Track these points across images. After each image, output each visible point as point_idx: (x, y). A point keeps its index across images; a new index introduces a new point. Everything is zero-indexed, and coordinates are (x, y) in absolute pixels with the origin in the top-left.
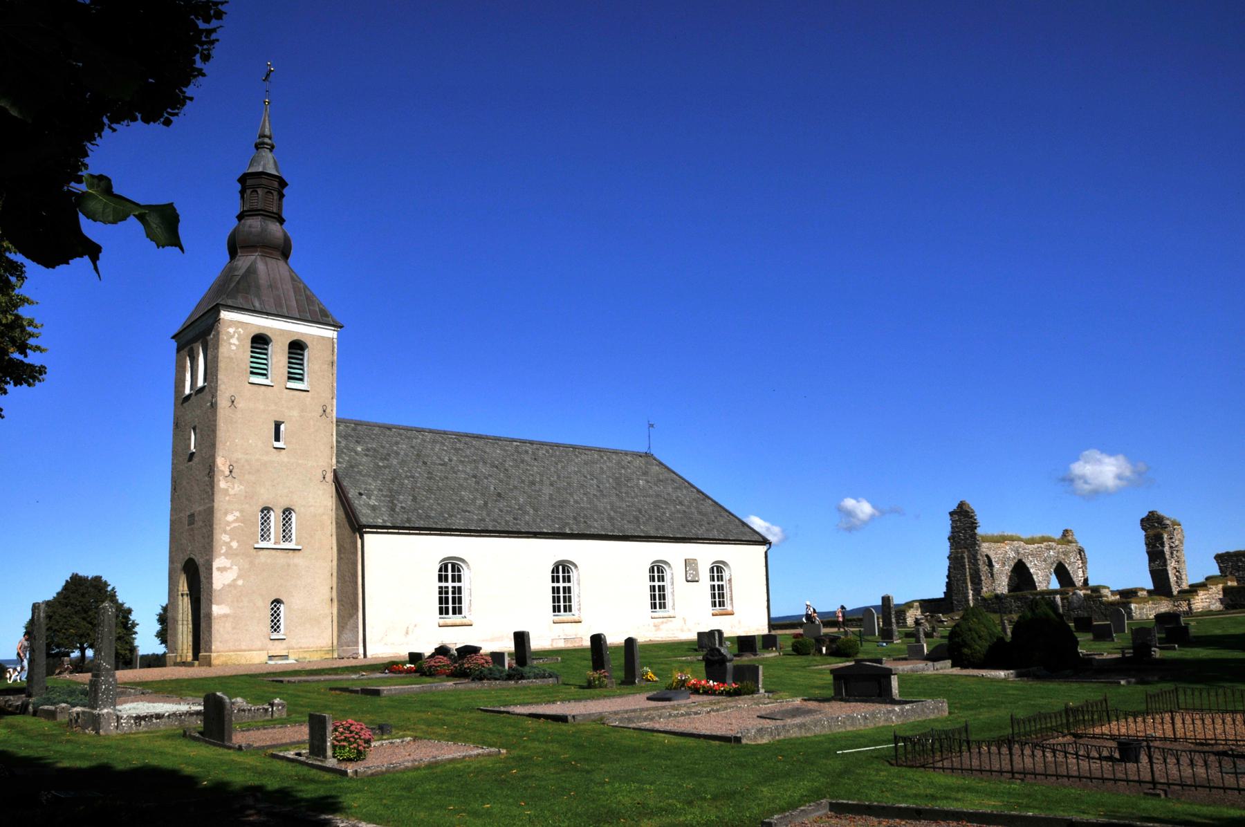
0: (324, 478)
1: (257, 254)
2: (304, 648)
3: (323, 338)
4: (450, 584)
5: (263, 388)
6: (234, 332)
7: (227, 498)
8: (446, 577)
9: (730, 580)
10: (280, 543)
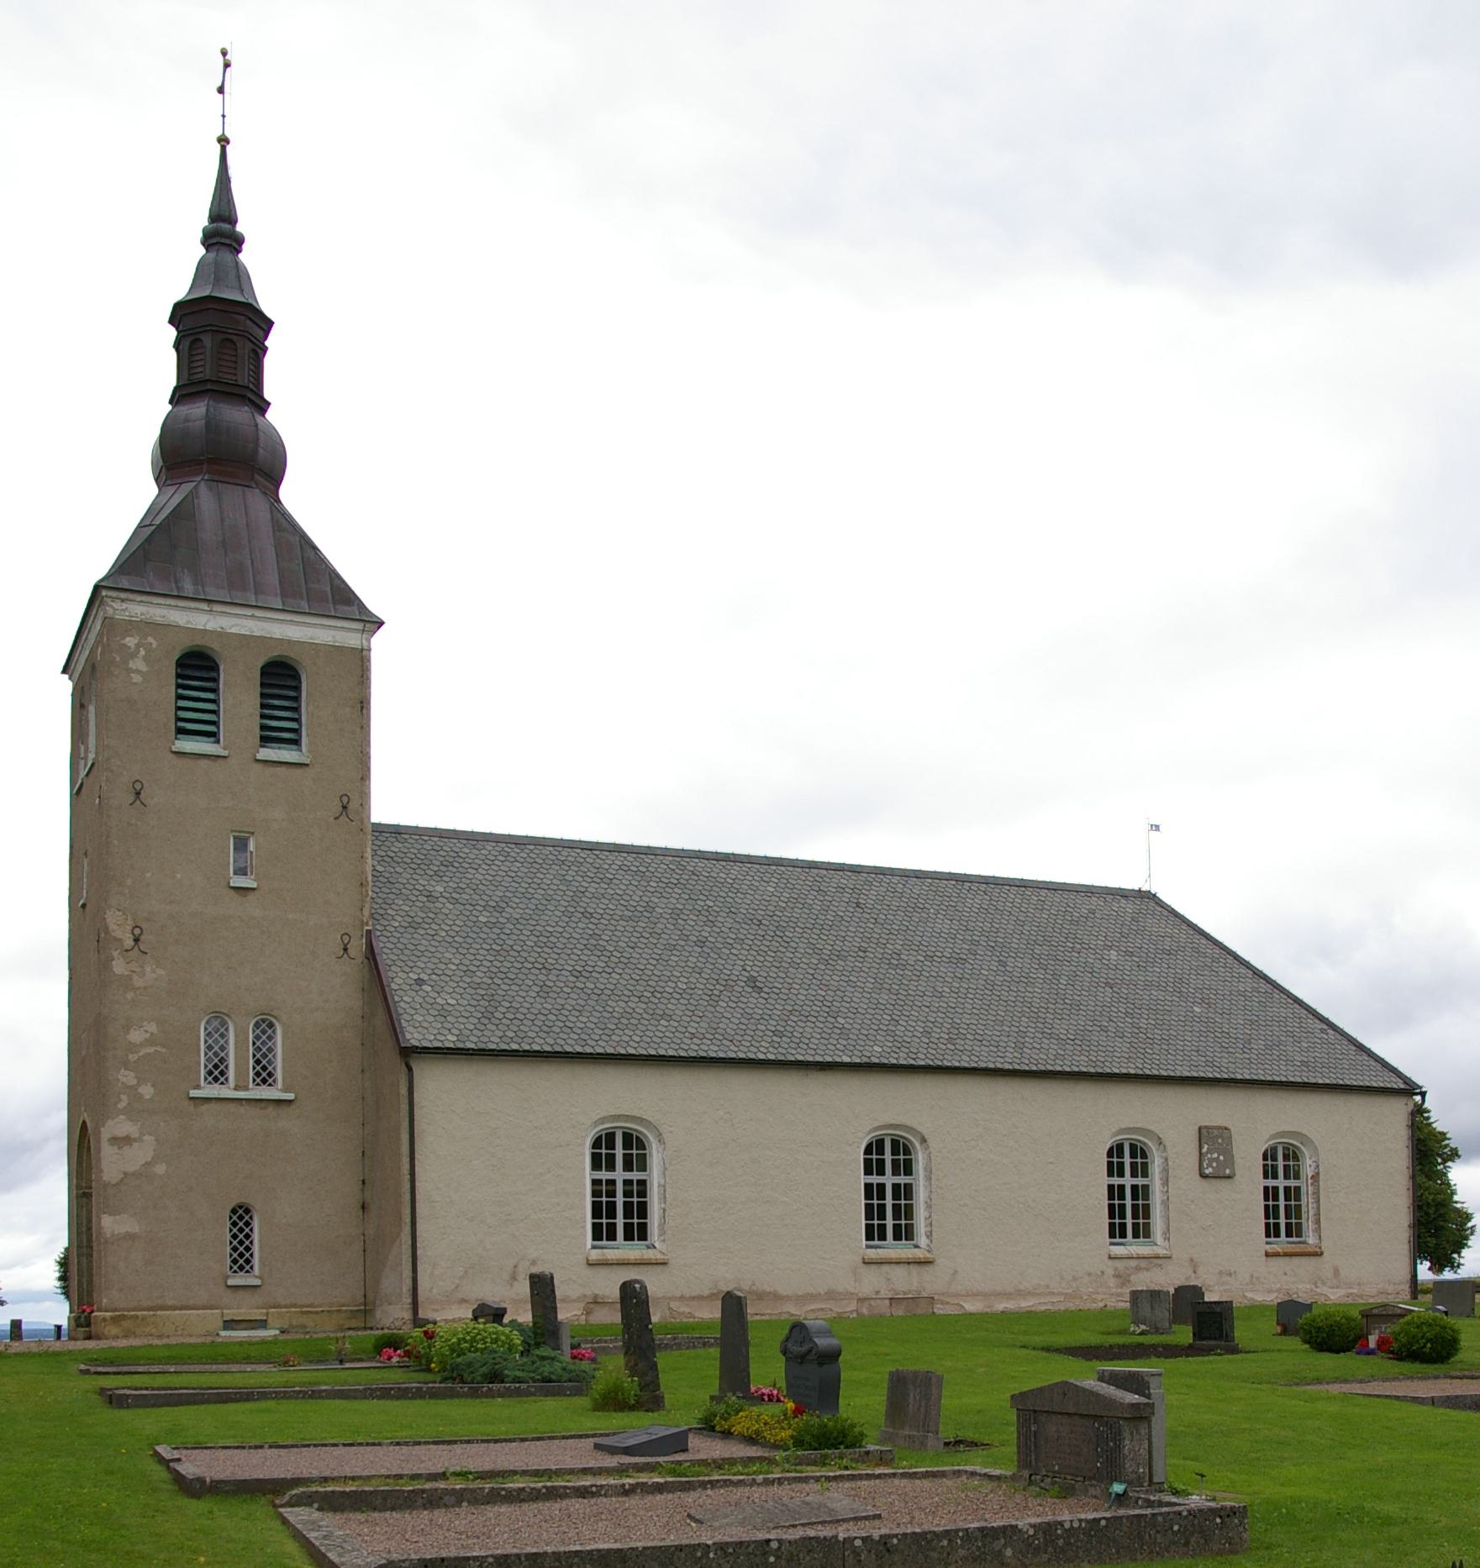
0: (345, 950)
1: (199, 478)
2: (301, 1306)
3: (340, 649)
4: (1128, 1181)
5: (204, 763)
6: (138, 646)
7: (130, 996)
8: (881, 1163)
9: (1316, 1177)
10: (246, 1088)
